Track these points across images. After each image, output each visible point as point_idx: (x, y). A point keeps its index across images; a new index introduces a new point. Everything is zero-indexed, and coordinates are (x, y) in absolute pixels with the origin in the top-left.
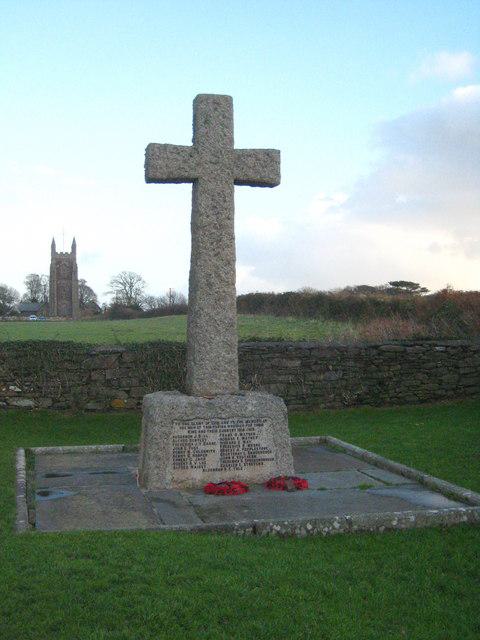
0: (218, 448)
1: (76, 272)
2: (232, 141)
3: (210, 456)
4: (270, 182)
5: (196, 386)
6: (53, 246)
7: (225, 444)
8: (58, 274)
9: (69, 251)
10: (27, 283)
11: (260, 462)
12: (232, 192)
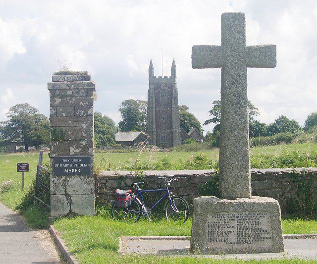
0: (235, 230)
1: (176, 98)
2: (244, 41)
3: (231, 235)
4: (272, 64)
5: (224, 193)
6: (151, 70)
7: (241, 230)
8: (157, 100)
9: (169, 75)
10: (121, 110)
11: (263, 240)
12: (245, 72)
